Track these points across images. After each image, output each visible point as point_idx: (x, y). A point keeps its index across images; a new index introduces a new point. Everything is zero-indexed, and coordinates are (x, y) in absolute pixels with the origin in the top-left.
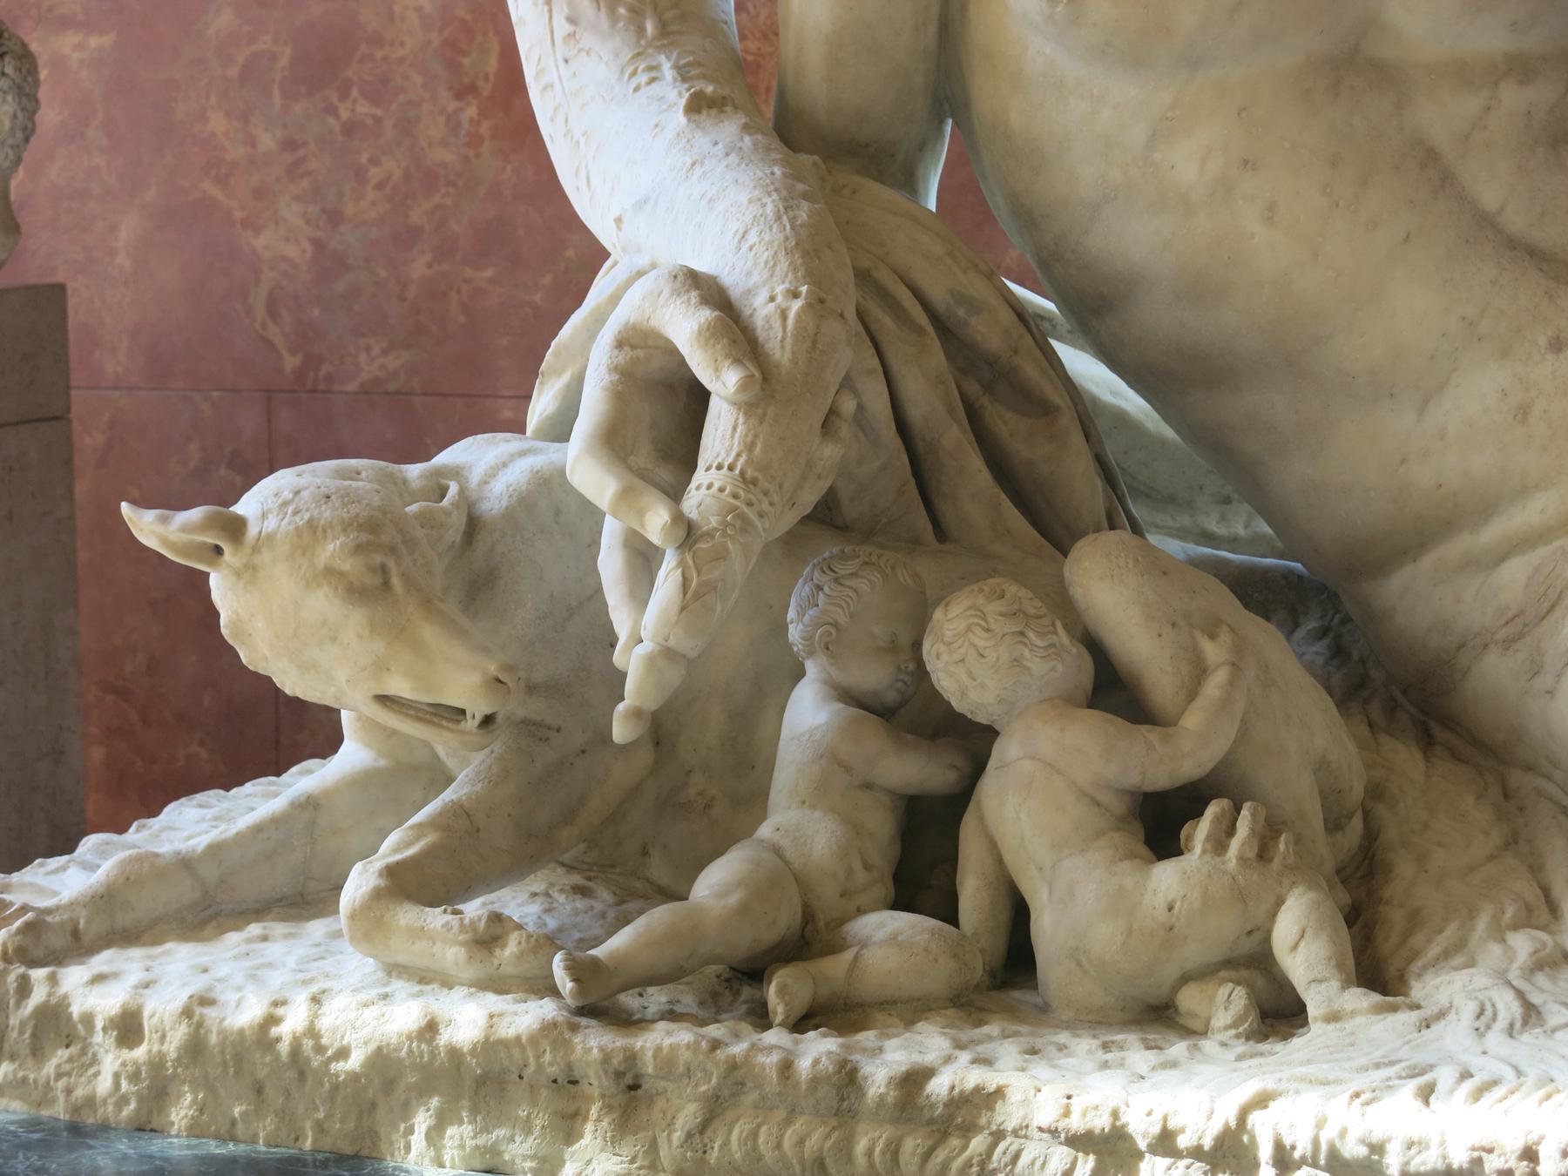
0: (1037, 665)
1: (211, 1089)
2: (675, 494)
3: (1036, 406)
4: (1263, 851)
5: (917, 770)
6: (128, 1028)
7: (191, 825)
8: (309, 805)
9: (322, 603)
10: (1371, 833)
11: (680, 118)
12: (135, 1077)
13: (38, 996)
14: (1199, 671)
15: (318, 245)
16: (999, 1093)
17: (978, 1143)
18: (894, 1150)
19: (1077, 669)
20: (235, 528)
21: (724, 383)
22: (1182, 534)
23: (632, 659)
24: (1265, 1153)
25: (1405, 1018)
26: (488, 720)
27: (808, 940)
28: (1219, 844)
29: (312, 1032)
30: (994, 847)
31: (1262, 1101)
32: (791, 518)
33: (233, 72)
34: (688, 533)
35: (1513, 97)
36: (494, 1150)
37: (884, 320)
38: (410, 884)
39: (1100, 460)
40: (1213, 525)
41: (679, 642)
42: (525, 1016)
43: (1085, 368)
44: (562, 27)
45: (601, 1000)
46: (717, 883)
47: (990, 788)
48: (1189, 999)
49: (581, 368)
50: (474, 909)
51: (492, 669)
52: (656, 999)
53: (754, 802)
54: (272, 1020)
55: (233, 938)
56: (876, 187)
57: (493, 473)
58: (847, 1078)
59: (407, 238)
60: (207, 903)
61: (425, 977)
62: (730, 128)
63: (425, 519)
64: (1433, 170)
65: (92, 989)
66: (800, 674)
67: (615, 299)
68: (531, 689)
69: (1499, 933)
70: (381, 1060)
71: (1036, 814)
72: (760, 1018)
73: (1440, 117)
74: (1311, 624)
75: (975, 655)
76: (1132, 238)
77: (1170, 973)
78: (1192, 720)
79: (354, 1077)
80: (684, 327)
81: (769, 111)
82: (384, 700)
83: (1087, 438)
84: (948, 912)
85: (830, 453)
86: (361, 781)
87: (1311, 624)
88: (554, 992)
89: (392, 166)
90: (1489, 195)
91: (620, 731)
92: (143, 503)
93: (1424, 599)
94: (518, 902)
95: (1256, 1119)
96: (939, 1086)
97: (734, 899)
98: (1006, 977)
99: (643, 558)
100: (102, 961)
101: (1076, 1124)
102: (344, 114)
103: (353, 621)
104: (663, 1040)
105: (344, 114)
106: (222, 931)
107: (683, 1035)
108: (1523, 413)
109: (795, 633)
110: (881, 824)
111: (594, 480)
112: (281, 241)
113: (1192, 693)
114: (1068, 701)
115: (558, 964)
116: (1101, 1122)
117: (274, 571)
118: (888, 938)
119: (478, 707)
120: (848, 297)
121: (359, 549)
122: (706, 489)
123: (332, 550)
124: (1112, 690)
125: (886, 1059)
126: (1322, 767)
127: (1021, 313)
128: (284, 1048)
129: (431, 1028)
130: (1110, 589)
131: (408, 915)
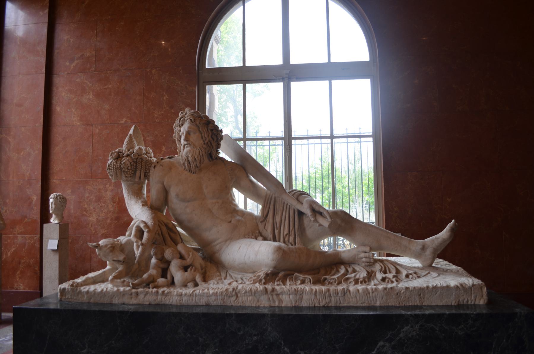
4: (195, 271)
5: (163, 266)
7: (91, 275)
8: (104, 272)
10: (205, 271)
13: (78, 290)
14: (189, 255)
15: (97, 219)
19: (178, 256)
21: (146, 231)
25: (207, 284)
28: (191, 270)
31: (194, 291)
43: (179, 229)
45: (134, 286)
46: (145, 276)
50: (122, 280)
58: (157, 292)
59: (107, 218)
60: (94, 281)
62: (146, 207)
65: (84, 289)
72: (149, 288)
75: (168, 254)
82: (114, 260)
84: (166, 278)
86: (109, 270)
89: (106, 211)
96: (166, 292)
99: (138, 247)
100: (85, 287)
104: (140, 290)
108: (218, 232)
110: (160, 270)
113: (188, 257)
118: (161, 280)
120: (157, 223)
124: (182, 257)
125: (161, 290)
126: (201, 264)
127: (173, 224)
131: (116, 280)
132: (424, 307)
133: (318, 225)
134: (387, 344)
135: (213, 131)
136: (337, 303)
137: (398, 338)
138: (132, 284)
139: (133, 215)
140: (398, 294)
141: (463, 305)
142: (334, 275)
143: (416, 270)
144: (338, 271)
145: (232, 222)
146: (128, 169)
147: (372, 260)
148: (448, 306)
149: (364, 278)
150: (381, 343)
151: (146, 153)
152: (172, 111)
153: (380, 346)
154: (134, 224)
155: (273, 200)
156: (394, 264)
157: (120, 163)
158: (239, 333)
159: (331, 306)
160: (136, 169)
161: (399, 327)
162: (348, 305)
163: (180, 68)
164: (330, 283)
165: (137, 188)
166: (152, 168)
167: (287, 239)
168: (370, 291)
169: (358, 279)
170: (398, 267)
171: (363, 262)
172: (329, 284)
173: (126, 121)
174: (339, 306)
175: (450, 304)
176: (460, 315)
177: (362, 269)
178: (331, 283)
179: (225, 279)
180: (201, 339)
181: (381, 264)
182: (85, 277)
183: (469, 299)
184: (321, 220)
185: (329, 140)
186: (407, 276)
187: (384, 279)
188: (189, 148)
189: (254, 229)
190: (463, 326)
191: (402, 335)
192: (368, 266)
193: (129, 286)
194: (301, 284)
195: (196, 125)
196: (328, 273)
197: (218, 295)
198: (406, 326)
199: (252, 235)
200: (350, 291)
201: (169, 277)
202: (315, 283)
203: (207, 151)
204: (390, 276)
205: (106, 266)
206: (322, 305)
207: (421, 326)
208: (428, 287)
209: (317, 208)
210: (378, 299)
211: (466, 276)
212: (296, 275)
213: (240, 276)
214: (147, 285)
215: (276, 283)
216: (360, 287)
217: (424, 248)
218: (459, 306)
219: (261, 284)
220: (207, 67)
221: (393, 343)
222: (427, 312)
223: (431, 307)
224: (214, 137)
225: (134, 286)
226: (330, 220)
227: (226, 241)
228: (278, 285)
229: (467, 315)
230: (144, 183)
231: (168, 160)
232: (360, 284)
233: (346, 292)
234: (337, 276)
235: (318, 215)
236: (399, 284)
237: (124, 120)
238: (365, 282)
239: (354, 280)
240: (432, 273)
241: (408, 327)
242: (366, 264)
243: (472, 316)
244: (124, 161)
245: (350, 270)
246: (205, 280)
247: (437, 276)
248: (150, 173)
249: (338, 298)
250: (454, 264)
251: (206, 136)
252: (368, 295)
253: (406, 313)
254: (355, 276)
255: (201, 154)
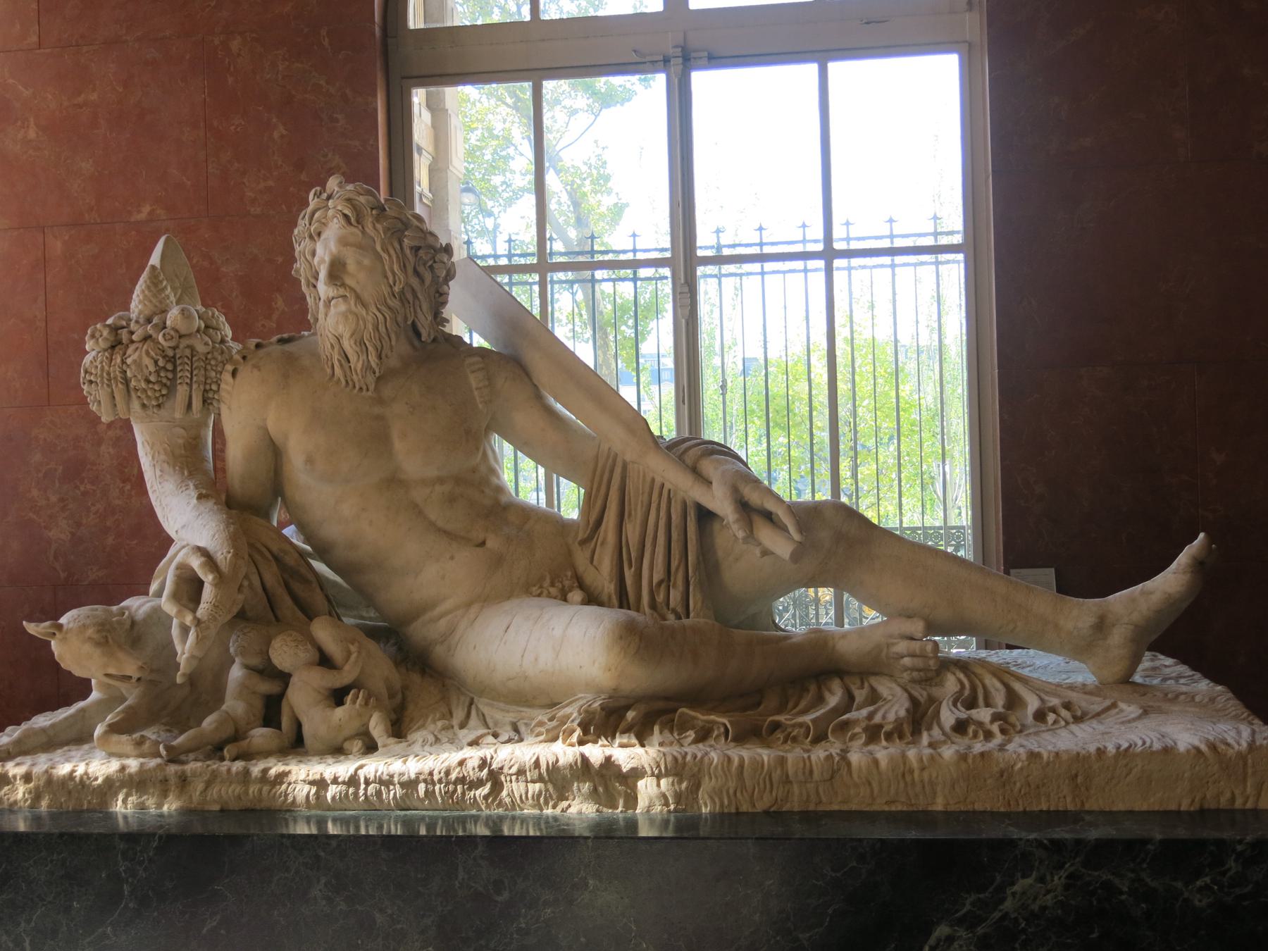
0: (302, 655)
1: (55, 795)
2: (194, 611)
3: (305, 581)
5: (266, 687)
6: (27, 778)
7: (42, 721)
8: (83, 710)
9: (87, 648)
10: (404, 699)
11: (195, 501)
12: (30, 793)
14: (349, 654)
15: (73, 534)
16: (289, 772)
17: (284, 787)
18: (260, 791)
19: (312, 655)
20: (60, 627)
22: (354, 617)
23: (182, 658)
24: (362, 780)
25: (404, 744)
26: (139, 679)
27: (237, 736)
28: (354, 702)
29: (86, 773)
30: (292, 708)
32: (229, 617)
33: (41, 475)
34: (198, 622)
35: (439, 489)
36: (143, 803)
37: (257, 557)
38: (114, 729)
39: (327, 596)
40: (364, 614)
41: (197, 653)
42: (153, 763)
44: (158, 473)
45: (175, 757)
46: (209, 722)
47: (290, 691)
48: (346, 745)
49: (166, 577)
50: (136, 736)
51: (140, 664)
52: (191, 756)
53: (220, 700)
54: (73, 771)
55: (59, 751)
56: (255, 518)
57: (139, 607)
58: (247, 772)
61: (120, 756)
62: (210, 504)
63: (119, 622)
64: (417, 510)
66: (233, 662)
67: (176, 555)
68: (152, 671)
69: (434, 722)
70: (109, 781)
71: (303, 696)
72: (222, 759)
73: (418, 495)
74: (392, 641)
75: (284, 653)
76: (332, 532)
77: (341, 738)
78: (347, 668)
79: (99, 786)
80: (196, 563)
81: (223, 497)
82: (107, 675)
83: (322, 589)
85: (241, 597)
86: (99, 703)
87: (392, 641)
88: (160, 756)
90: (433, 517)
91: (179, 680)
92: (30, 620)
93: (420, 631)
94: (151, 733)
95: (360, 772)
96: (273, 772)
97: (214, 726)
98: (296, 746)
99: (185, 630)
100: (18, 760)
101: (311, 778)
102: (82, 488)
103: (97, 653)
104: (193, 766)
105: (82, 488)
106: (55, 749)
107: (199, 764)
108: (443, 578)
109: (232, 650)
110: (258, 704)
111: (169, 607)
112: (59, 532)
114: (310, 664)
115: (161, 747)
116: (318, 777)
117: (72, 640)
118: (260, 735)
119: (136, 675)
121: (99, 631)
122: (203, 609)
123: (90, 632)
124: (325, 661)
125: (256, 769)
128: (77, 779)
129: (123, 768)
130: (323, 632)
131: (115, 738)
132: (1088, 818)
133: (757, 552)
134: (962, 933)
135: (421, 253)
136: (808, 800)
137: (997, 915)
138: (168, 748)
139: (172, 534)
140: (1005, 775)
141: (1218, 811)
142: (805, 712)
143: (1074, 696)
144: (820, 700)
145: (489, 544)
146: (148, 381)
147: (932, 662)
148: (1166, 813)
149: (899, 724)
150: (942, 930)
151: (207, 327)
152: (303, 177)
153: (939, 940)
154: (178, 556)
155: (618, 470)
156: (1000, 672)
157: (123, 362)
158: (499, 899)
159: (791, 813)
160: (175, 378)
161: (999, 879)
162: (845, 808)
163: (323, 32)
164: (791, 739)
165: (181, 441)
166: (227, 377)
167: (660, 598)
168: (915, 765)
169: (880, 727)
170: (1017, 686)
171: (906, 669)
172: (785, 741)
173: (151, 213)
174: (815, 812)
175: (1173, 807)
176: (1201, 844)
177: (898, 690)
178: (795, 739)
179: (462, 726)
180: (379, 918)
181: (962, 676)
182: (24, 726)
183: (1237, 792)
184: (767, 535)
185: (820, 264)
186: (1040, 716)
187: (961, 727)
188: (343, 307)
189: (549, 565)
190: (1208, 879)
191: (1008, 905)
192: (919, 682)
193: (159, 755)
194: (696, 741)
195: (364, 232)
196: (790, 705)
197: (436, 778)
198: (1024, 877)
199: (552, 585)
200: (849, 764)
201: (285, 722)
202: (741, 738)
203: (400, 319)
204: (983, 714)
205: (90, 691)
206: (760, 807)
207: (1069, 877)
208: (1101, 752)
209: (754, 498)
210: (939, 788)
211: (1236, 718)
212: (683, 714)
213: (510, 717)
214: (216, 751)
215: (618, 741)
216: (883, 753)
217: (1101, 626)
218: (1203, 815)
219: (572, 745)
220: (411, 25)
221: (980, 930)
222: (1093, 834)
223: (1111, 817)
224: (421, 269)
225: (175, 757)
226: (796, 537)
227: (469, 605)
228: (622, 746)
229: (1220, 843)
230: (206, 425)
231: (279, 347)
232: (884, 743)
233: (838, 768)
234: (813, 716)
235: (759, 523)
236: (1010, 741)
237: (146, 209)
238: (901, 737)
239: (866, 730)
240: (1122, 705)
241: (1029, 881)
242: (915, 674)
243: (1239, 848)
244: (135, 356)
245: (860, 695)
246: (398, 730)
247: (1139, 718)
248: (223, 393)
249: (811, 786)
250: (1207, 675)
251: (396, 267)
252: (908, 778)
253: (1024, 835)
254: (870, 716)
255: (382, 329)
